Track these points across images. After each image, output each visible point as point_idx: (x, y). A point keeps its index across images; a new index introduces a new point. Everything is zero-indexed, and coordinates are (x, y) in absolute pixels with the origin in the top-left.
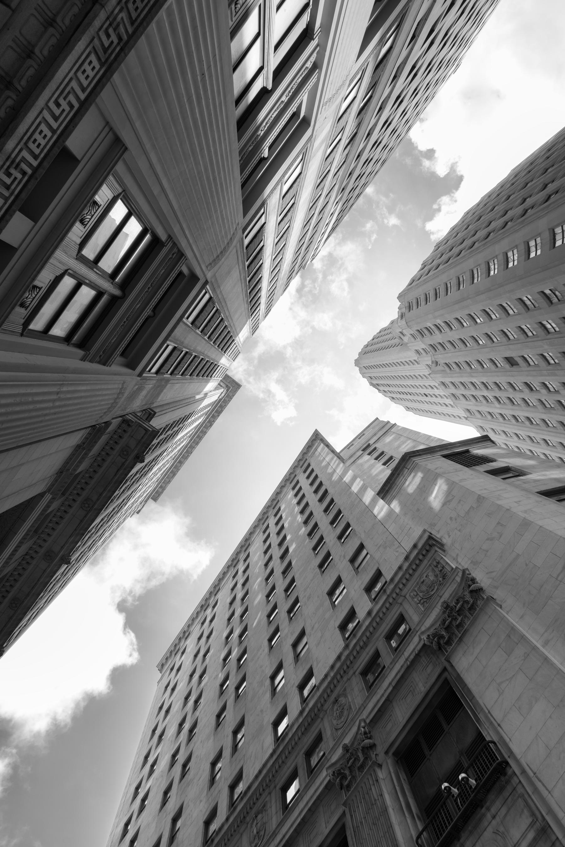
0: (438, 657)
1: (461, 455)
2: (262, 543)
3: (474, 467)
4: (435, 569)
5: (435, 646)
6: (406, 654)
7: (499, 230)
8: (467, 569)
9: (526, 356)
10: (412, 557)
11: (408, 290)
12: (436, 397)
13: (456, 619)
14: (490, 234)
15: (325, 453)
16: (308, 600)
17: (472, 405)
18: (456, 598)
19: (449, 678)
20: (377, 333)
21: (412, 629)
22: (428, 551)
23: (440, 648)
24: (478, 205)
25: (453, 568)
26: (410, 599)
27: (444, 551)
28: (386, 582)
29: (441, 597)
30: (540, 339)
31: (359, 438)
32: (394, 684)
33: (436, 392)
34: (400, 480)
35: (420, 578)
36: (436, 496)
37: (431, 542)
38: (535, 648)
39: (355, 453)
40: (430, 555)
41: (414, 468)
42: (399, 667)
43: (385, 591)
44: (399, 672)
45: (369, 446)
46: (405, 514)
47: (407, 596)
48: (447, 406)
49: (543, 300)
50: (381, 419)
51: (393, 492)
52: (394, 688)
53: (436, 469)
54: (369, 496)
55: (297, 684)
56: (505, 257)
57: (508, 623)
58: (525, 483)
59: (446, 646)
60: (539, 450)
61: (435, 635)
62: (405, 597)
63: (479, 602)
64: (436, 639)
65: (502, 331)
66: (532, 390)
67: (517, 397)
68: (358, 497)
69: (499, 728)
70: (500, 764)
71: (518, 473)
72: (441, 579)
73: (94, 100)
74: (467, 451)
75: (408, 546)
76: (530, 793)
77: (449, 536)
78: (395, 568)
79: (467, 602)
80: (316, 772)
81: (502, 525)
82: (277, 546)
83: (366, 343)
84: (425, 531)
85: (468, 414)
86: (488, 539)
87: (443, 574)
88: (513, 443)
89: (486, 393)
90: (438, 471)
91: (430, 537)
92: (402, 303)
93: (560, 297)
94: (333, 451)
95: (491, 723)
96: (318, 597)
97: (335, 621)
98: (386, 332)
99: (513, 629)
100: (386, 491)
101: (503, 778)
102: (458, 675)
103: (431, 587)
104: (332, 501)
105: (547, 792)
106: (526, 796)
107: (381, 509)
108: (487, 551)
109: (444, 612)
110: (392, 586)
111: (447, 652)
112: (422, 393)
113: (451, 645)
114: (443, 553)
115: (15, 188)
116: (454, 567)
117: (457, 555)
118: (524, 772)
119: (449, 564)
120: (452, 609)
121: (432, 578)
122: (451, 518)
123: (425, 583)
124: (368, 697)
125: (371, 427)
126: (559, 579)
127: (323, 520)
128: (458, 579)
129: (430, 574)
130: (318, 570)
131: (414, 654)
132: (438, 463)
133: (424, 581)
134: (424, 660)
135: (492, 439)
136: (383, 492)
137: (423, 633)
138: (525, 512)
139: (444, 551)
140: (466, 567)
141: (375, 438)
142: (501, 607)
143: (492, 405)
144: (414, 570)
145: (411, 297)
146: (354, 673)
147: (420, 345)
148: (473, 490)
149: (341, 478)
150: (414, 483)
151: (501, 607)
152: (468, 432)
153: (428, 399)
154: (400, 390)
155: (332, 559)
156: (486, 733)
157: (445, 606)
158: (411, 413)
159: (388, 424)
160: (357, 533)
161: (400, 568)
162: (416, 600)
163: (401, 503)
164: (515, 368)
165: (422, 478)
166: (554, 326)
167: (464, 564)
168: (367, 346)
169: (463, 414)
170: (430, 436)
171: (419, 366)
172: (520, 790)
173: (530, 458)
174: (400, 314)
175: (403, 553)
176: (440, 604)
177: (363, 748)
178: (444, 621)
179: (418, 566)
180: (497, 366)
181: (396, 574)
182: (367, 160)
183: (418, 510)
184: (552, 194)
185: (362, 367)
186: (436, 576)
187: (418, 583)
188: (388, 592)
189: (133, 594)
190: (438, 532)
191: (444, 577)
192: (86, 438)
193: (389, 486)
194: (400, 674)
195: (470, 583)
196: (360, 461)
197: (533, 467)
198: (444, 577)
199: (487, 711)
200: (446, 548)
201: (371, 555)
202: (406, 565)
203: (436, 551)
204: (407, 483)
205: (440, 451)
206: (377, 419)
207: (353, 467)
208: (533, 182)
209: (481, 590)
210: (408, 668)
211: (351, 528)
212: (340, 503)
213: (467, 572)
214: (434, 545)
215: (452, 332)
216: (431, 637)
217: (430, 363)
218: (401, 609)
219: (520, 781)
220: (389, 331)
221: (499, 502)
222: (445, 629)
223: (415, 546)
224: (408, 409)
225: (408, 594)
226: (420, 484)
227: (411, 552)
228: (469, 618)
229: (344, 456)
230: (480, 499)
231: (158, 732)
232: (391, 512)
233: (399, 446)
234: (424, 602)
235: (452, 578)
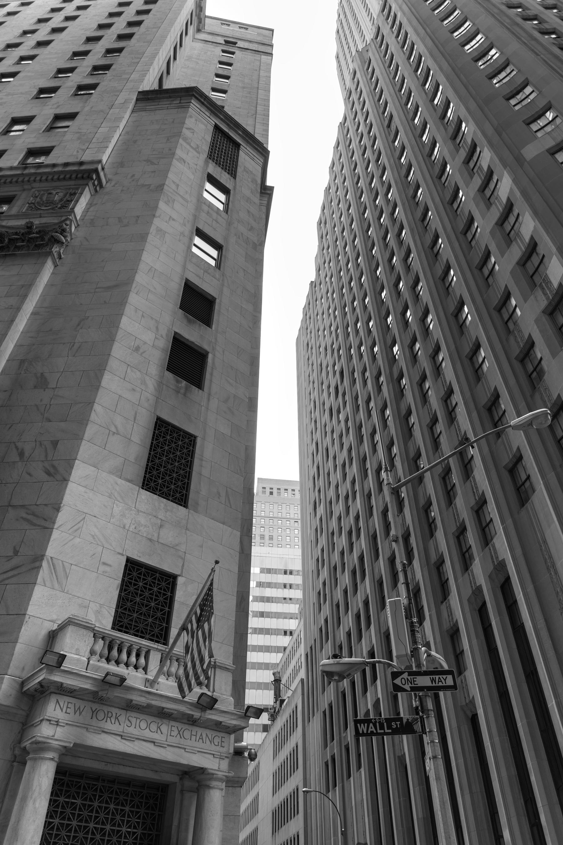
2: (49, 9)
40: (81, 182)
67: (368, 153)
72: (59, 206)
74: (238, 146)
81: (137, 221)
82: (116, 36)
96: (5, 112)
121: (57, 198)
123: (50, 196)
126: (97, 290)
129: (61, 194)
144: (59, 179)
157: (29, 225)
159: (269, 48)
160: (88, 102)
162: (32, 198)
176: (28, 220)
177: (52, 236)
179: (64, 179)
183: (135, 142)
186: (61, 200)
191: (63, 207)
193: (154, 96)
202: (60, 169)
206: (272, 31)
229: (209, 25)
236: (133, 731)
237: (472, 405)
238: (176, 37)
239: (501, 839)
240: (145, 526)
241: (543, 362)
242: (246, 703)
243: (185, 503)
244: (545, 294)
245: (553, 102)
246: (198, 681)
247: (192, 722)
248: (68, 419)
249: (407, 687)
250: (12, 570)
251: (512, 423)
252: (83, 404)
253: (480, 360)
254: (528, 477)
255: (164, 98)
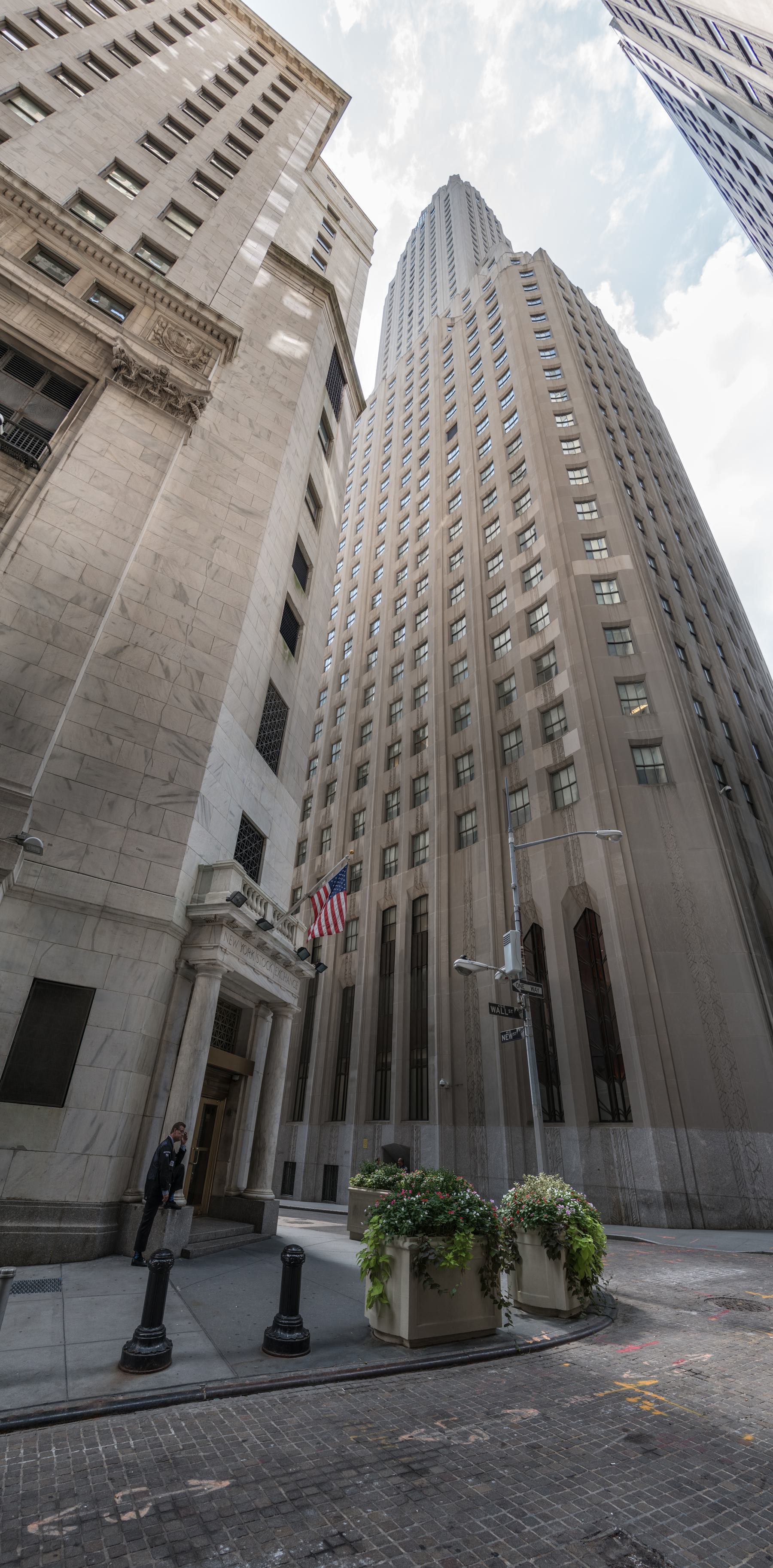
0: (105, 368)
1: (339, 375)
3: (327, 393)
4: (200, 351)
5: (115, 362)
6: (91, 319)
7: (598, 400)
8: (212, 397)
9: (458, 449)
10: (205, 314)
11: (549, 267)
12: (409, 331)
13: (154, 388)
14: (590, 368)
15: (316, 125)
16: (93, 115)
17: (401, 383)
18: (177, 386)
19: (89, 386)
20: (495, 217)
21: (122, 325)
22: (197, 323)
23: (116, 370)
24: (633, 369)
25: (207, 377)
26: (155, 318)
27: (224, 363)
28: (164, 274)
29: (171, 364)
30: (494, 713)
31: (345, 199)
32: (49, 303)
33: (415, 330)
34: (297, 281)
35: (184, 330)
36: (285, 343)
37: (229, 340)
38: (157, 487)
39: (323, 192)
41: (315, 302)
42: (73, 311)
43: (152, 273)
44: (67, 310)
45: (337, 219)
46: (255, 296)
47: (157, 313)
48: (398, 348)
49: (541, 647)
50: (376, 237)
51: (281, 272)
52: (46, 304)
53: (319, 338)
54: (265, 225)
55: (268, 842)
56: (622, 625)
57: (171, 454)
58: (318, 460)
59: (120, 377)
60: (355, 476)
61: (126, 359)
62: (156, 309)
63: (181, 416)
64: (123, 362)
65: (487, 416)
66: (421, 460)
68: (263, 207)
69: (66, 456)
70: (34, 462)
71: (327, 451)
72: (191, 362)
73: (555, 766)
75: (217, 305)
76: (25, 497)
77: (242, 368)
78: (186, 287)
79: (177, 402)
80: (716, 651)
81: (269, 437)
83: (482, 196)
84: (241, 329)
85: (389, 380)
86: (250, 420)
87: (197, 365)
88: (360, 444)
89: (416, 401)
90: (317, 341)
91: (235, 340)
92: (533, 257)
93: (516, 482)
94: (321, 144)
95: (67, 446)
96: (106, 139)
97: (85, 180)
98: (495, 233)
99: (168, 461)
100: (279, 257)
101: (22, 465)
102: (97, 399)
103: (180, 349)
104: (112, 74)
105: (34, 514)
106: (20, 494)
107: (254, 252)
108: (238, 421)
109: (156, 371)
110: (162, 285)
111: (115, 380)
112: (414, 307)
113: (125, 385)
114: (221, 361)
115: (19, 501)
116: (210, 379)
117: (224, 382)
118: (40, 488)
119: (210, 371)
120: (163, 381)
122: (263, 368)
123: (180, 338)
124: (16, 259)
125: (364, 221)
127: (225, 121)
128: (198, 386)
130: (84, 51)
131: (95, 332)
132: (327, 341)
133: (182, 336)
134: (94, 347)
135: (362, 414)
136: (277, 253)
137: (123, 342)
138: (288, 463)
139: (224, 363)
140: (214, 395)
141: (348, 231)
142: (185, 445)
143: (402, 411)
145: (541, 275)
146: (35, 230)
147: (477, 295)
148: (301, 394)
149: (284, 166)
150: (297, 305)
151: (185, 445)
152: (368, 385)
153: (406, 318)
154: (417, 269)
155: (106, 81)
156: (55, 441)
157: (164, 371)
158: (385, 291)
159: (368, 252)
161: (187, 296)
163: (268, 286)
164: (444, 436)
165: (305, 318)
166: (494, 536)
167: (218, 392)
168: (478, 198)
169: (389, 372)
170: (358, 326)
171: (449, 298)
172: (22, 486)
173: (346, 465)
174: (518, 256)
175: (206, 299)
176: (164, 364)
178: (147, 372)
180: (447, 413)
181: (179, 290)
182: (748, 194)
184: (643, 484)
185: (449, 191)
186: (193, 355)
187: (177, 327)
188: (153, 279)
189: (39, 386)
190: (244, 352)
192: (738, 656)
194: (65, 313)
195: (198, 403)
196: (313, 204)
197: (336, 469)
198: (194, 366)
199: (76, 439)
200: (228, 365)
201: (190, 242)
203: (221, 350)
204: (295, 294)
205: (342, 341)
206: (428, 1119)
207: (304, 192)
208: (639, 438)
209: (196, 418)
210: (77, 325)
211: (217, 197)
212: (248, 166)
213: (209, 397)
214: (227, 347)
215: (490, 346)
216: (123, 355)
217: (452, 315)
218: (139, 304)
219: (29, 485)
220: (497, 239)
221: (292, 430)
222: (139, 374)
223: (219, 317)
224: (392, 286)
225: (159, 314)
226: (296, 314)
227: (211, 311)
228: (160, 406)
230: (292, 405)
231: (683, 502)
232: (252, 271)
233: (341, 275)
234: (158, 339)
235: (198, 378)
236: (259, 967)
237: (443, 749)
238: (342, 487)
239: (388, 1072)
240: (206, 267)
241: (469, 718)
242: (437, 1129)
243: (626, 1118)
244: (554, 755)
245: (608, 534)
246: (204, 1149)
247: (287, 965)
248: (122, 855)
249: (519, 989)
250: (169, 796)
251: (244, 1185)
252: (224, 643)
253: (422, 693)
254: (426, 789)
255: (297, 273)
